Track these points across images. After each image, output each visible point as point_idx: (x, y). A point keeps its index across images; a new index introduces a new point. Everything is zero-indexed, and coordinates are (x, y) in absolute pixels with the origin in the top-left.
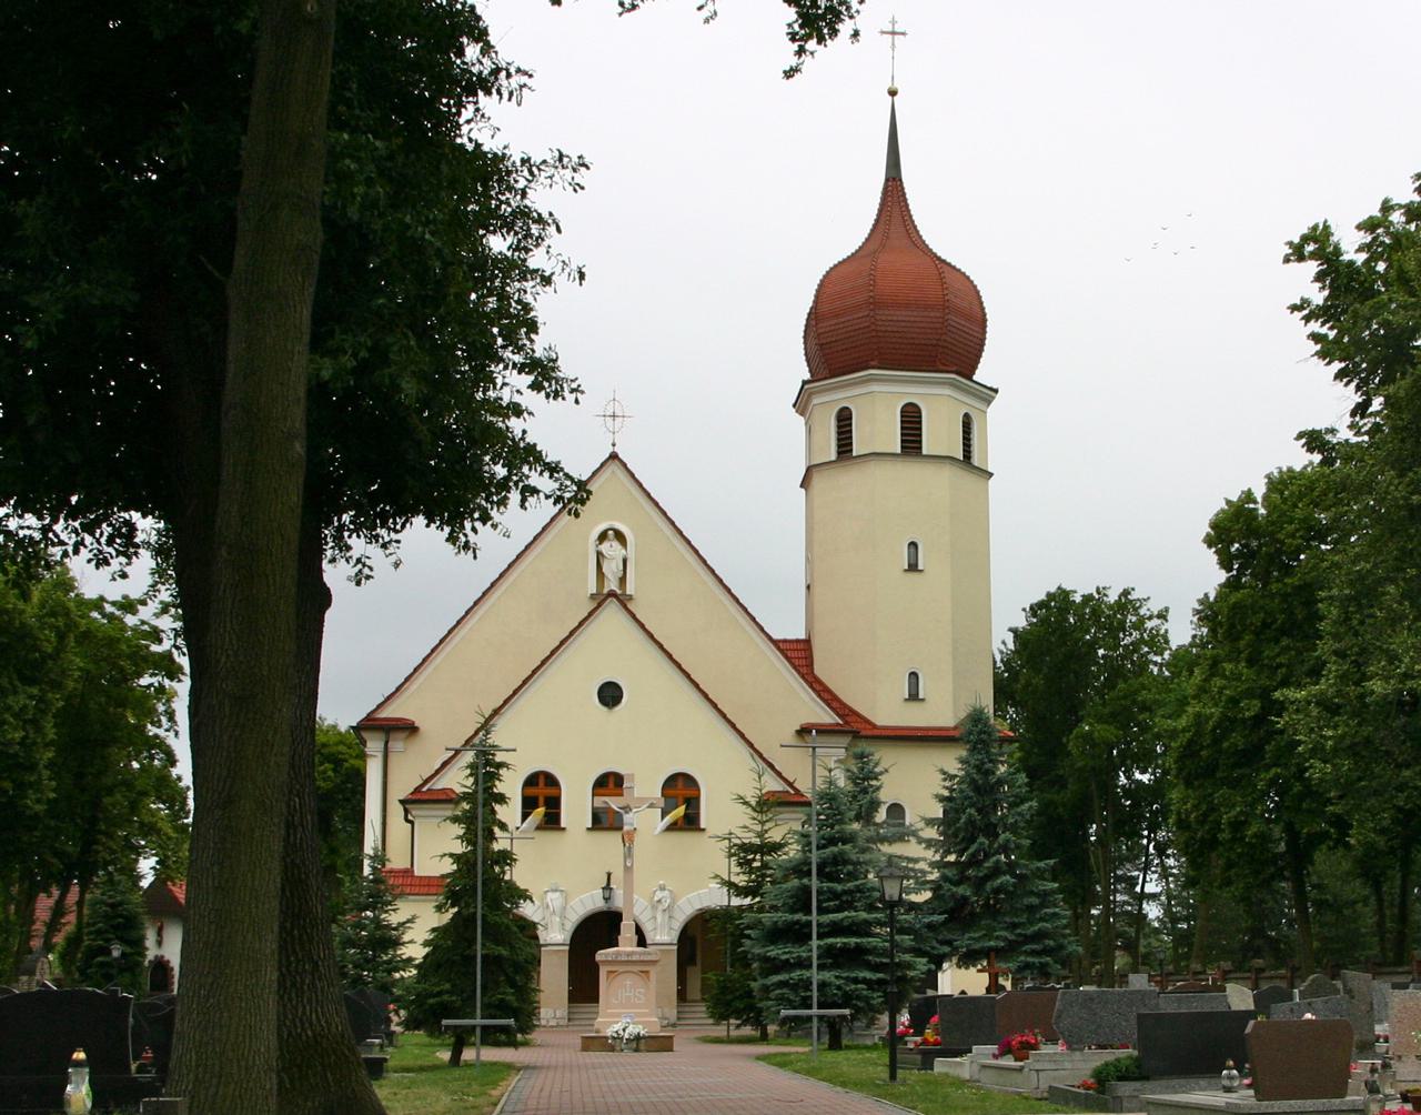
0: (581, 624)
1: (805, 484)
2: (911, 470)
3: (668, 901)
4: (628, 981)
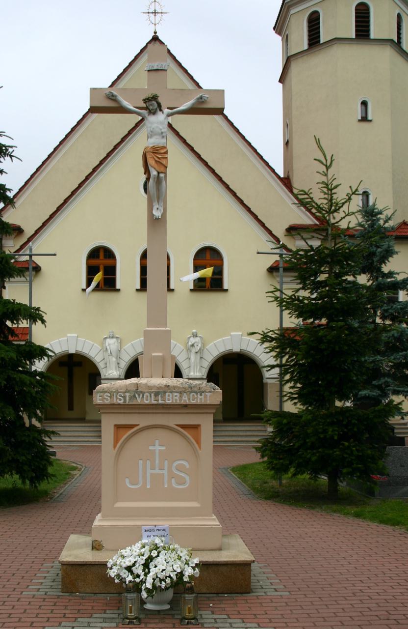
0: (130, 133)
1: (282, 80)
2: (362, 51)
3: (200, 345)
4: (157, 445)
